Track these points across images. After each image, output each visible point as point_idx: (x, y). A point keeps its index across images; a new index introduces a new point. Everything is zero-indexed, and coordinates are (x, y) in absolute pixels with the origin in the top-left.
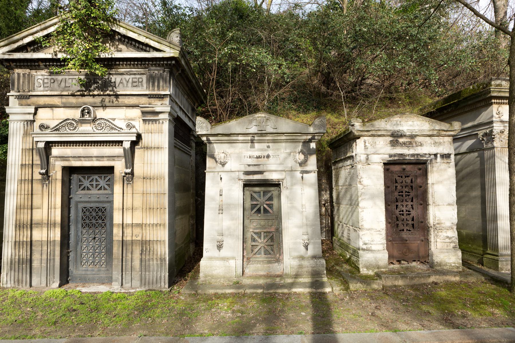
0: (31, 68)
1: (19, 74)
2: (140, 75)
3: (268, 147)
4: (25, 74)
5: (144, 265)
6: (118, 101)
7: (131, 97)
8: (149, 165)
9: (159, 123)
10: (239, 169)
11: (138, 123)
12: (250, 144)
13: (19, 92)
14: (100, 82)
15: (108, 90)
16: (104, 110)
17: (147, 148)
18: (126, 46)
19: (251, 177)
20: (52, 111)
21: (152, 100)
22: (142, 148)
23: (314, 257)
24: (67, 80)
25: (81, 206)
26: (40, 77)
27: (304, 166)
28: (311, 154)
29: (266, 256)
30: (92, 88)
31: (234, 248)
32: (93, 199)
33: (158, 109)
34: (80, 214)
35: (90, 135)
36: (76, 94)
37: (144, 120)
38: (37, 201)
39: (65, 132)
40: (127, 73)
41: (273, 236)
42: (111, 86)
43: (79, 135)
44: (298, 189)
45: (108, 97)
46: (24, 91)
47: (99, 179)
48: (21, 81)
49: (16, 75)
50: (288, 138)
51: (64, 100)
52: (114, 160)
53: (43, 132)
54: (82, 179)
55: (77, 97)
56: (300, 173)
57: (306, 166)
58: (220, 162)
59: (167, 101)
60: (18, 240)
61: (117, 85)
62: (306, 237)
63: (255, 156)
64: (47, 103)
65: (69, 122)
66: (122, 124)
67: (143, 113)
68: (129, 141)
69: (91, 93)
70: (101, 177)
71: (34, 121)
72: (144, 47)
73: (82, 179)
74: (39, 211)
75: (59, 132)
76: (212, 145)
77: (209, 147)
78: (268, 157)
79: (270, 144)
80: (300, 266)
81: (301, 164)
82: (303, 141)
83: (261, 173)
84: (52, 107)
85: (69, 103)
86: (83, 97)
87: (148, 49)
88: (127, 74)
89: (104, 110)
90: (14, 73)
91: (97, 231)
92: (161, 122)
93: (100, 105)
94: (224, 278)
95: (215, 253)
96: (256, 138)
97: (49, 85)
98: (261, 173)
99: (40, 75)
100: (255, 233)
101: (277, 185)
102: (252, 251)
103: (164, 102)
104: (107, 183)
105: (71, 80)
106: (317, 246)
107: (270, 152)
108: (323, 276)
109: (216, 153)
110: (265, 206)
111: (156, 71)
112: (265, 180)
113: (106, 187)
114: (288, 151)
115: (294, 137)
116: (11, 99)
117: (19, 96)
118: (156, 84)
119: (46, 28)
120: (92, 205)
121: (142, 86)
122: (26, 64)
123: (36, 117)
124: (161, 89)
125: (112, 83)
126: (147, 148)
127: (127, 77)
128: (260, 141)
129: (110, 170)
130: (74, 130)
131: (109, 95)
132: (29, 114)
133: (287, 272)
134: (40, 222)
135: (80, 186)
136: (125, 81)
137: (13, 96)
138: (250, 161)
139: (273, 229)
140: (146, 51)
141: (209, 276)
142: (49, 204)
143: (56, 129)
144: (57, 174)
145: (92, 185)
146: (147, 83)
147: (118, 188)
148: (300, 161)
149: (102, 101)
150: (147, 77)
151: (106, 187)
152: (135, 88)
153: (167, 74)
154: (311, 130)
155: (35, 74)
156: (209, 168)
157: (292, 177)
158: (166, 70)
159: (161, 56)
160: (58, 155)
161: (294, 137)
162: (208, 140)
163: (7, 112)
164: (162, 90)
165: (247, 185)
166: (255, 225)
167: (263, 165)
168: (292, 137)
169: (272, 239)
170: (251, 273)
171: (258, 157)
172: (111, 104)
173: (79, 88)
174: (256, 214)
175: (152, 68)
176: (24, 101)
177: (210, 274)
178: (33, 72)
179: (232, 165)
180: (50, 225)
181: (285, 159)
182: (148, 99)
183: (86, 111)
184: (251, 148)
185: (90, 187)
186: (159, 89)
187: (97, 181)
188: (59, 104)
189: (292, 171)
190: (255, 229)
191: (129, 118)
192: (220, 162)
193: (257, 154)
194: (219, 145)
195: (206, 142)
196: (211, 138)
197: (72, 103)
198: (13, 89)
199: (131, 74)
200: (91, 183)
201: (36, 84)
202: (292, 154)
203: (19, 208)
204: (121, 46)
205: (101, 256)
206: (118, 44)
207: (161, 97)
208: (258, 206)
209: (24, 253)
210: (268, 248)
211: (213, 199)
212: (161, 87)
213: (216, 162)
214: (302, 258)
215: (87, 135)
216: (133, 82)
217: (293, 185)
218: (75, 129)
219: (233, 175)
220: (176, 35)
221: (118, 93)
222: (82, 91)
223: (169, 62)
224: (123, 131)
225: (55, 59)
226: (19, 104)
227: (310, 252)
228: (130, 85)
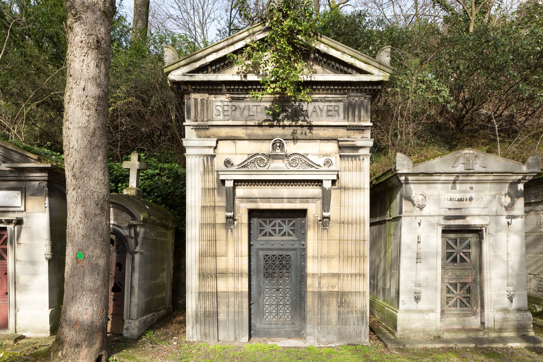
3: (471, 188)
5: (342, 320)
6: (312, 133)
7: (326, 128)
8: (346, 208)
9: (360, 160)
10: (438, 213)
11: (334, 158)
12: (451, 185)
13: (196, 121)
14: (290, 110)
15: (299, 120)
16: (294, 144)
17: (346, 189)
18: (322, 66)
19: (452, 222)
20: (234, 144)
21: (351, 133)
22: (338, 188)
23: (519, 310)
24: (251, 107)
25: (261, 253)
26: (220, 104)
27: (510, 210)
28: (518, 197)
29: (462, 309)
30: (281, 118)
31: (433, 298)
32: (276, 246)
33: (359, 143)
34: (262, 263)
35: (284, 173)
36: (264, 124)
37: (340, 156)
38: (221, 248)
39: (255, 169)
41: (470, 287)
42: (303, 115)
43: (272, 173)
44: (502, 236)
45: (300, 128)
46: (202, 121)
47: (282, 224)
48: (199, 107)
49: (192, 101)
50: (496, 178)
51: (249, 131)
52: (307, 202)
53: (229, 169)
54: (263, 223)
55: (263, 128)
56: (507, 218)
57: (513, 210)
58: (418, 205)
59: (368, 134)
60: (201, 291)
61: (309, 115)
62: (511, 288)
63: (457, 199)
65: (258, 157)
66: (320, 161)
67: (340, 147)
68: (329, 180)
69: (281, 124)
70: (284, 222)
71: (214, 156)
72: (345, 69)
73: (263, 223)
74: (224, 258)
76: (408, 186)
77: (405, 187)
78: (471, 199)
79: (473, 185)
80: (505, 320)
81: (507, 208)
82: (511, 181)
83: (463, 217)
84: (234, 139)
85: (255, 135)
86: (271, 128)
87: (350, 70)
88: (321, 101)
89: (294, 144)
90: (190, 98)
91: (281, 282)
92: (361, 158)
93: (291, 137)
94: (423, 331)
95: (413, 305)
96: (460, 178)
97: (229, 113)
98: (463, 217)
99: (220, 102)
100: (451, 284)
101: (478, 232)
102: (447, 303)
103: (365, 135)
104: (291, 228)
105: (255, 107)
106: (523, 298)
107: (473, 195)
108: (529, 330)
109: (413, 195)
110: (462, 254)
111: (356, 98)
112: (468, 225)
113: (291, 232)
114: (493, 193)
115: (502, 178)
116: (187, 129)
119: (233, 44)
120: (275, 253)
123: (216, 150)
124: (362, 119)
125: (303, 111)
126: (346, 189)
127: (321, 105)
128: (463, 182)
129: (303, 213)
130: (264, 166)
131: (302, 126)
132: (210, 147)
133: (490, 326)
134: (225, 271)
135: (261, 231)
136: (321, 110)
137: (190, 126)
138: (450, 205)
139: (469, 280)
140: (346, 73)
141: (407, 330)
142: (235, 252)
143: (243, 166)
144: (243, 217)
145: (274, 231)
146: (344, 112)
147: (312, 236)
148: (506, 205)
149: (293, 133)
151: (291, 232)
152: (330, 118)
153: (368, 101)
154: (524, 169)
155: (214, 99)
156: (405, 212)
157: (497, 223)
158: (367, 96)
159: (368, 80)
160: (244, 196)
161: (502, 178)
162: (407, 180)
163: (184, 145)
164: (363, 121)
165: (446, 231)
166: (450, 275)
167: (465, 208)
168: (500, 177)
169: (469, 291)
170: (446, 327)
171: (461, 200)
172: (303, 137)
173: (265, 117)
174: (451, 264)
175: (352, 94)
176: (202, 132)
177: (409, 327)
178: (212, 98)
179: (430, 209)
180: (237, 274)
181: (491, 201)
182: (346, 132)
183: (278, 145)
184: (452, 189)
185: (272, 233)
186: (360, 120)
187: (280, 225)
188: (244, 136)
189: (497, 215)
190: (449, 279)
191: (324, 153)
192: (418, 205)
193: (458, 196)
194: (416, 185)
195: (403, 182)
196: (410, 178)
197: (258, 135)
198: (189, 118)
199: (326, 101)
200: (273, 228)
201: (215, 112)
202: (497, 196)
203: (203, 255)
204: (316, 67)
205: (286, 308)
206: (313, 65)
207: (361, 129)
208: (455, 255)
209: (209, 305)
210: (464, 301)
211: (409, 247)
212: (362, 117)
213: (414, 205)
214: (506, 310)
215: (282, 173)
217: (497, 231)
218: (265, 165)
219: (432, 219)
220: (386, 54)
221: (314, 123)
222: (269, 120)
223: (375, 87)
224: (321, 169)
225: (244, 81)
226: (197, 135)
227: (514, 305)
228: (324, 114)
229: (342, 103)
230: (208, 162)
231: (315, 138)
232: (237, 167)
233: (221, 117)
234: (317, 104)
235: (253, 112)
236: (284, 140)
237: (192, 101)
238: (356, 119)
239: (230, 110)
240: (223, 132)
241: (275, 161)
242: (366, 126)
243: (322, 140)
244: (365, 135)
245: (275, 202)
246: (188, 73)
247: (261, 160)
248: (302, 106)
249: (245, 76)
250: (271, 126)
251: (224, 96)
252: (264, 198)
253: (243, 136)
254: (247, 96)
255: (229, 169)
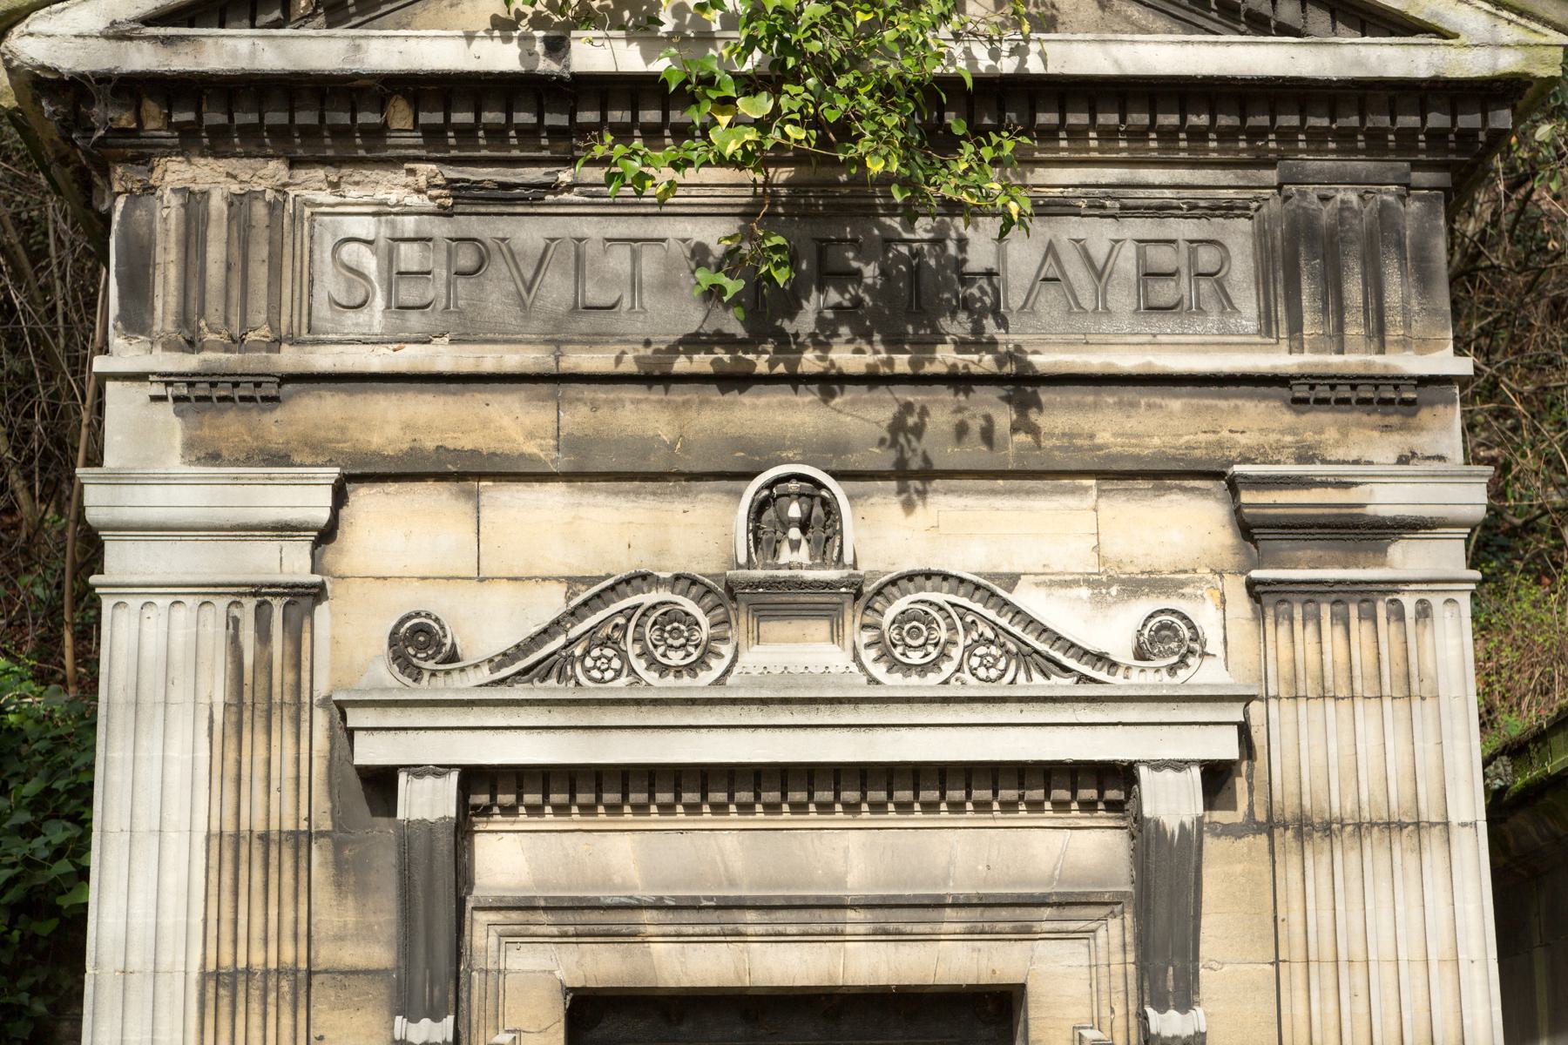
0: (302, 148)
1: (194, 201)
2: (1218, 221)
4: (252, 196)
6: (1034, 430)
8: (1323, 976)
9: (1398, 614)
13: (192, 345)
14: (870, 272)
15: (938, 338)
16: (909, 506)
20: (469, 507)
21: (1323, 427)
22: (1251, 826)
24: (590, 250)
26: (363, 227)
30: (805, 322)
33: (1386, 499)
36: (681, 365)
37: (1256, 591)
39: (621, 687)
40: (1098, 205)
42: (966, 304)
45: (945, 394)
46: (237, 343)
48: (216, 252)
49: (168, 213)
52: (1024, 932)
53: (426, 689)
55: (679, 394)
59: (1444, 430)
61: (1014, 299)
64: (430, 444)
65: (649, 598)
67: (1248, 529)
68: (1179, 765)
69: (810, 362)
71: (317, 593)
75: (566, 691)
84: (467, 472)
86: (732, 396)
88: (1098, 209)
89: (909, 506)
90: (149, 190)
92: (1409, 602)
93: (884, 459)
97: (434, 290)
99: (366, 215)
103: (1423, 442)
105: (623, 252)
111: (1342, 189)
117: (190, 379)
118: (1354, 290)
121: (1226, 303)
122: (276, 118)
123: (330, 554)
124: (1394, 333)
125: (966, 279)
127: (1099, 234)
130: (692, 669)
131: (959, 381)
132: (284, 530)
136: (1088, 275)
137: (140, 377)
143: (535, 664)
146: (1263, 281)
149: (897, 426)
150: (1262, 237)
152: (1168, 323)
153: (1431, 212)
155: (325, 197)
158: (1418, 177)
159: (1423, 73)
164: (1405, 344)
172: (973, 453)
173: (694, 318)
175: (1314, 164)
176: (232, 426)
178: (312, 186)
182: (1288, 418)
183: (795, 511)
188: (539, 449)
197: (646, 445)
198: (136, 322)
199: (1128, 211)
201: (329, 284)
207: (1394, 399)
216: (1150, 275)
218: (702, 662)
221: (1045, 360)
222: (723, 340)
224: (1117, 683)
226: (189, 445)
228: (1122, 299)
229: (1244, 225)
230: (264, 635)
231: (1061, 461)
232: (485, 675)
233: (375, 317)
234: (1067, 230)
235: (603, 282)
236: (838, 476)
237: (168, 213)
238: (1354, 331)
239: (441, 273)
240: (390, 422)
241: (771, 628)
242: (1423, 381)
243: (1119, 474)
244: (1423, 442)
245: (778, 937)
246: (148, 21)
247: (671, 618)
248: (962, 243)
249: (557, 46)
250: (735, 380)
251: (401, 177)
252: (693, 906)
253: (531, 448)
254: (565, 176)
255: (426, 689)
